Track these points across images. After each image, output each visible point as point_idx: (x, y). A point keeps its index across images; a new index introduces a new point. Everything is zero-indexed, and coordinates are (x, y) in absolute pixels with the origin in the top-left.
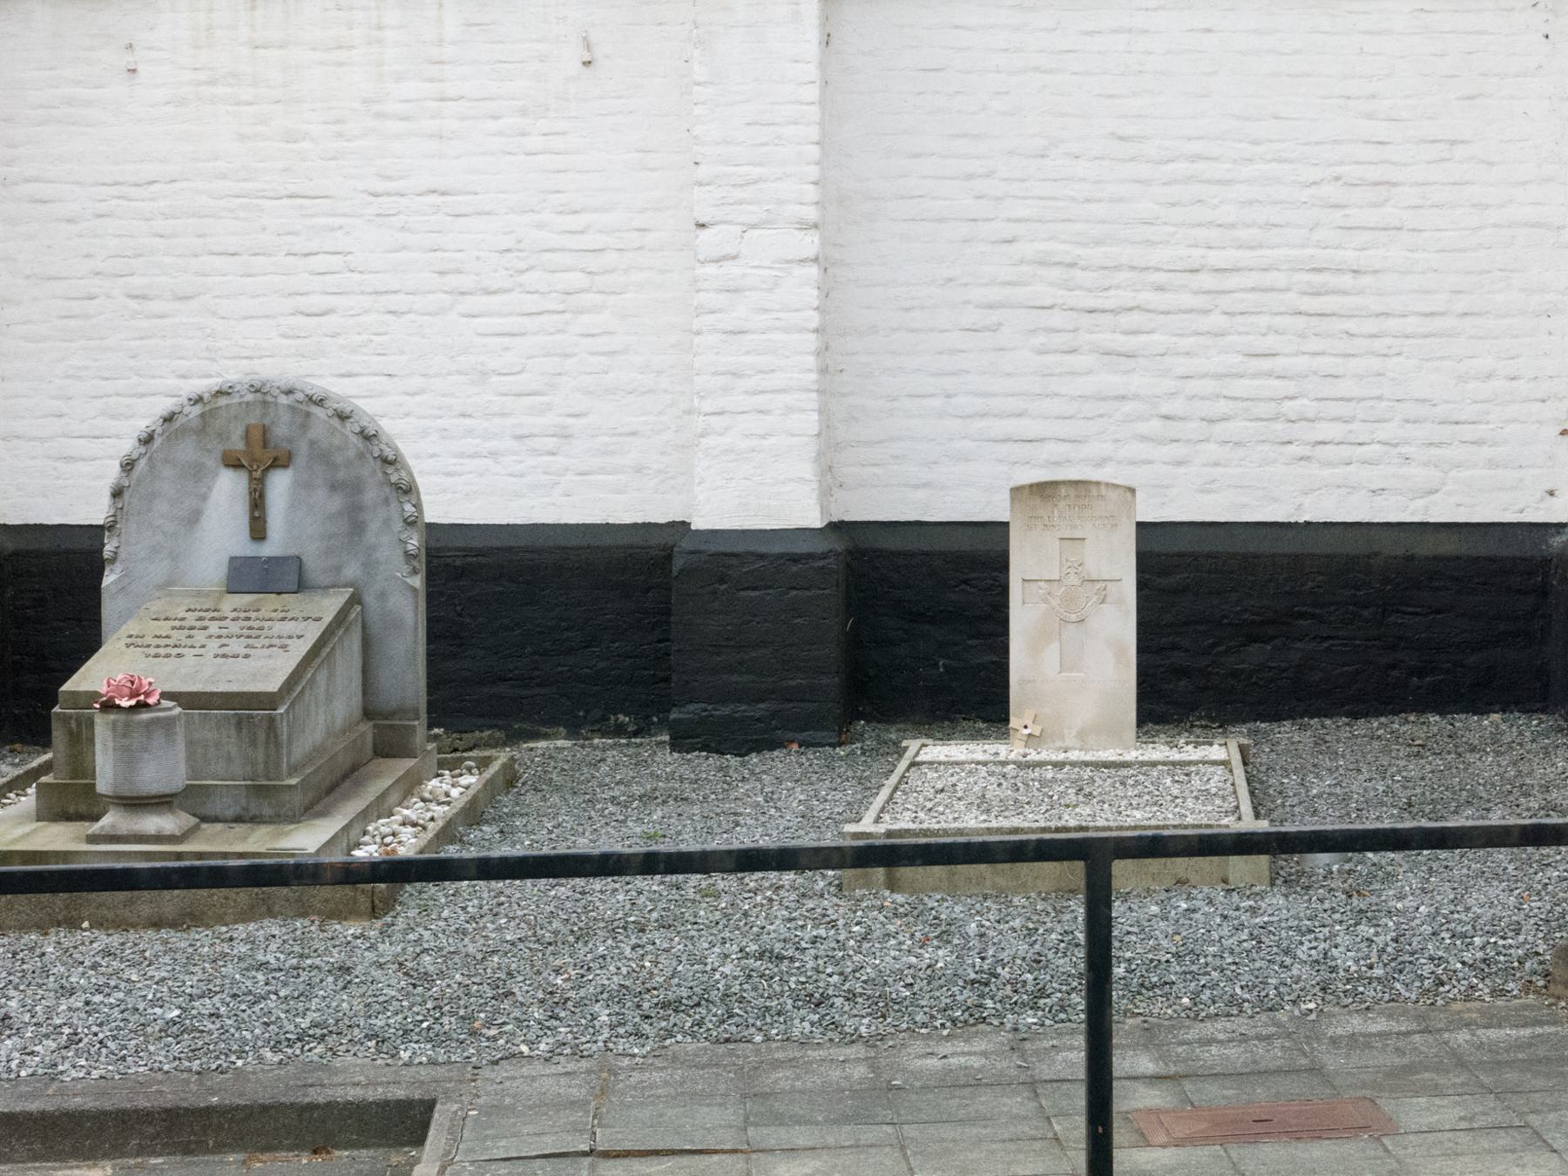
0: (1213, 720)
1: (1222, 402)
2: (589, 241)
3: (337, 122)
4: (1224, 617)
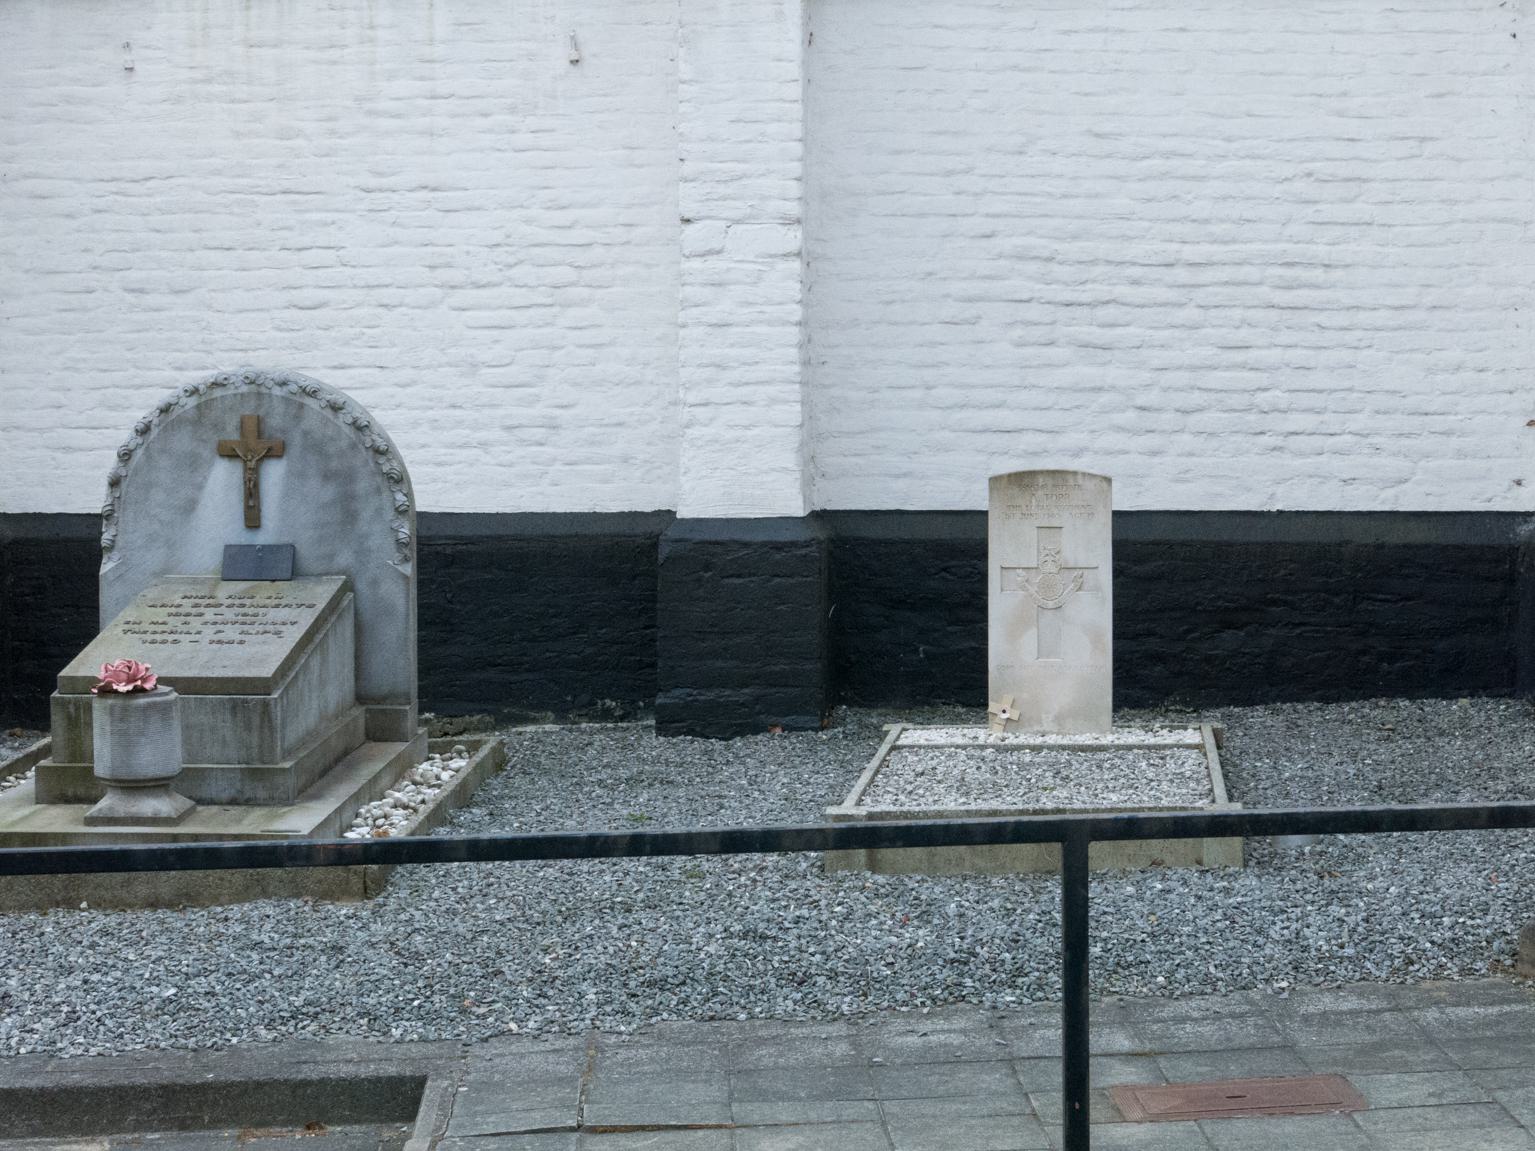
1: (1197, 393)
3: (330, 119)
4: (1197, 604)
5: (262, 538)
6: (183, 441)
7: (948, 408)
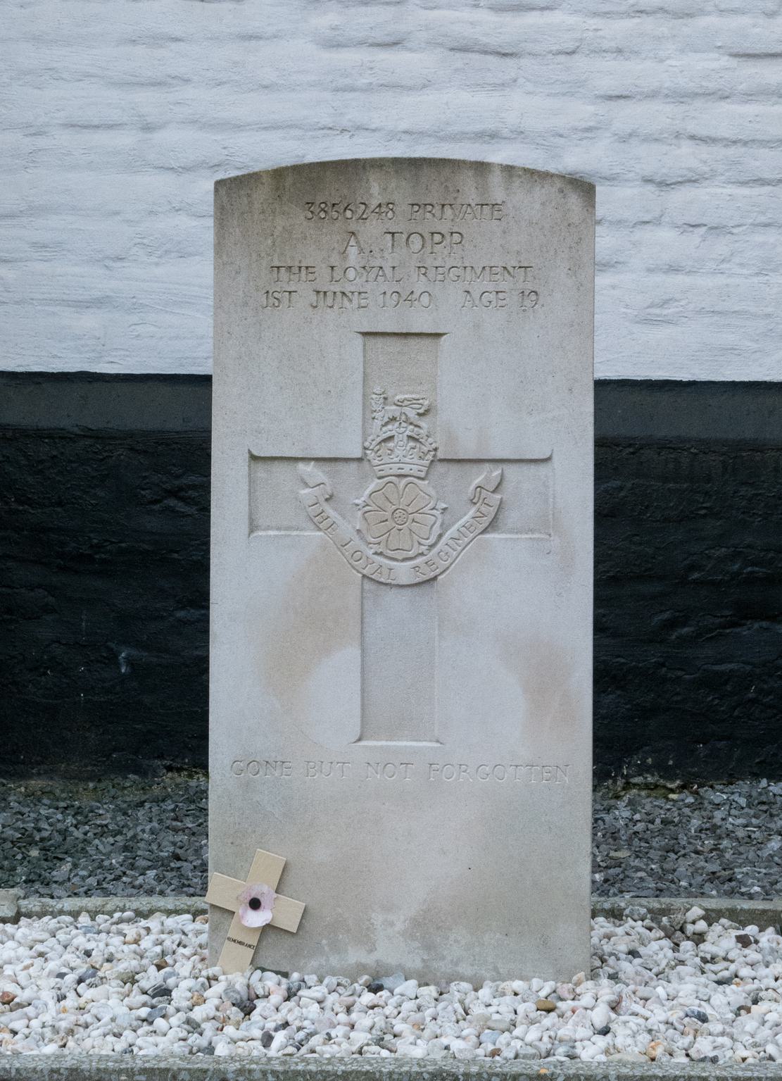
0: (668, 774)
1: (686, 147)
4: (693, 568)
7: (186, 169)
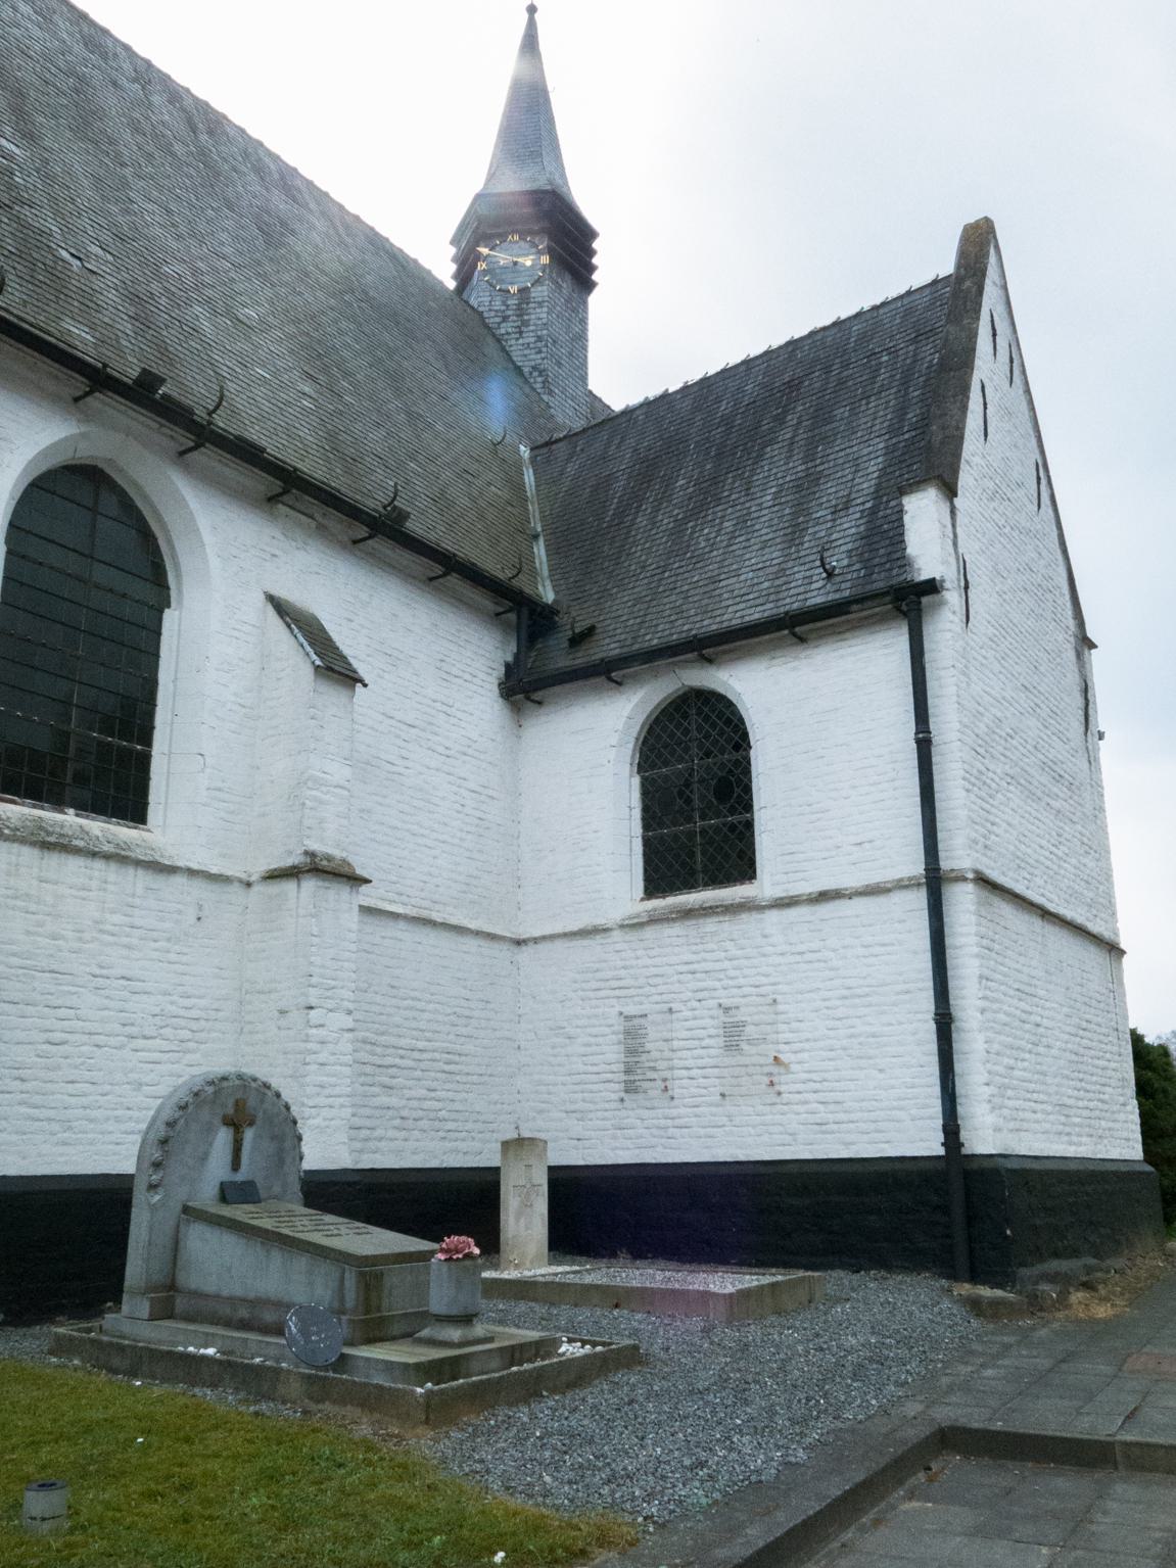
2: (194, 1013)
3: (79, 931)
5: (240, 1177)
6: (205, 1114)
